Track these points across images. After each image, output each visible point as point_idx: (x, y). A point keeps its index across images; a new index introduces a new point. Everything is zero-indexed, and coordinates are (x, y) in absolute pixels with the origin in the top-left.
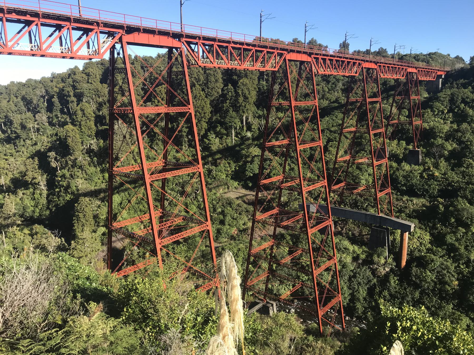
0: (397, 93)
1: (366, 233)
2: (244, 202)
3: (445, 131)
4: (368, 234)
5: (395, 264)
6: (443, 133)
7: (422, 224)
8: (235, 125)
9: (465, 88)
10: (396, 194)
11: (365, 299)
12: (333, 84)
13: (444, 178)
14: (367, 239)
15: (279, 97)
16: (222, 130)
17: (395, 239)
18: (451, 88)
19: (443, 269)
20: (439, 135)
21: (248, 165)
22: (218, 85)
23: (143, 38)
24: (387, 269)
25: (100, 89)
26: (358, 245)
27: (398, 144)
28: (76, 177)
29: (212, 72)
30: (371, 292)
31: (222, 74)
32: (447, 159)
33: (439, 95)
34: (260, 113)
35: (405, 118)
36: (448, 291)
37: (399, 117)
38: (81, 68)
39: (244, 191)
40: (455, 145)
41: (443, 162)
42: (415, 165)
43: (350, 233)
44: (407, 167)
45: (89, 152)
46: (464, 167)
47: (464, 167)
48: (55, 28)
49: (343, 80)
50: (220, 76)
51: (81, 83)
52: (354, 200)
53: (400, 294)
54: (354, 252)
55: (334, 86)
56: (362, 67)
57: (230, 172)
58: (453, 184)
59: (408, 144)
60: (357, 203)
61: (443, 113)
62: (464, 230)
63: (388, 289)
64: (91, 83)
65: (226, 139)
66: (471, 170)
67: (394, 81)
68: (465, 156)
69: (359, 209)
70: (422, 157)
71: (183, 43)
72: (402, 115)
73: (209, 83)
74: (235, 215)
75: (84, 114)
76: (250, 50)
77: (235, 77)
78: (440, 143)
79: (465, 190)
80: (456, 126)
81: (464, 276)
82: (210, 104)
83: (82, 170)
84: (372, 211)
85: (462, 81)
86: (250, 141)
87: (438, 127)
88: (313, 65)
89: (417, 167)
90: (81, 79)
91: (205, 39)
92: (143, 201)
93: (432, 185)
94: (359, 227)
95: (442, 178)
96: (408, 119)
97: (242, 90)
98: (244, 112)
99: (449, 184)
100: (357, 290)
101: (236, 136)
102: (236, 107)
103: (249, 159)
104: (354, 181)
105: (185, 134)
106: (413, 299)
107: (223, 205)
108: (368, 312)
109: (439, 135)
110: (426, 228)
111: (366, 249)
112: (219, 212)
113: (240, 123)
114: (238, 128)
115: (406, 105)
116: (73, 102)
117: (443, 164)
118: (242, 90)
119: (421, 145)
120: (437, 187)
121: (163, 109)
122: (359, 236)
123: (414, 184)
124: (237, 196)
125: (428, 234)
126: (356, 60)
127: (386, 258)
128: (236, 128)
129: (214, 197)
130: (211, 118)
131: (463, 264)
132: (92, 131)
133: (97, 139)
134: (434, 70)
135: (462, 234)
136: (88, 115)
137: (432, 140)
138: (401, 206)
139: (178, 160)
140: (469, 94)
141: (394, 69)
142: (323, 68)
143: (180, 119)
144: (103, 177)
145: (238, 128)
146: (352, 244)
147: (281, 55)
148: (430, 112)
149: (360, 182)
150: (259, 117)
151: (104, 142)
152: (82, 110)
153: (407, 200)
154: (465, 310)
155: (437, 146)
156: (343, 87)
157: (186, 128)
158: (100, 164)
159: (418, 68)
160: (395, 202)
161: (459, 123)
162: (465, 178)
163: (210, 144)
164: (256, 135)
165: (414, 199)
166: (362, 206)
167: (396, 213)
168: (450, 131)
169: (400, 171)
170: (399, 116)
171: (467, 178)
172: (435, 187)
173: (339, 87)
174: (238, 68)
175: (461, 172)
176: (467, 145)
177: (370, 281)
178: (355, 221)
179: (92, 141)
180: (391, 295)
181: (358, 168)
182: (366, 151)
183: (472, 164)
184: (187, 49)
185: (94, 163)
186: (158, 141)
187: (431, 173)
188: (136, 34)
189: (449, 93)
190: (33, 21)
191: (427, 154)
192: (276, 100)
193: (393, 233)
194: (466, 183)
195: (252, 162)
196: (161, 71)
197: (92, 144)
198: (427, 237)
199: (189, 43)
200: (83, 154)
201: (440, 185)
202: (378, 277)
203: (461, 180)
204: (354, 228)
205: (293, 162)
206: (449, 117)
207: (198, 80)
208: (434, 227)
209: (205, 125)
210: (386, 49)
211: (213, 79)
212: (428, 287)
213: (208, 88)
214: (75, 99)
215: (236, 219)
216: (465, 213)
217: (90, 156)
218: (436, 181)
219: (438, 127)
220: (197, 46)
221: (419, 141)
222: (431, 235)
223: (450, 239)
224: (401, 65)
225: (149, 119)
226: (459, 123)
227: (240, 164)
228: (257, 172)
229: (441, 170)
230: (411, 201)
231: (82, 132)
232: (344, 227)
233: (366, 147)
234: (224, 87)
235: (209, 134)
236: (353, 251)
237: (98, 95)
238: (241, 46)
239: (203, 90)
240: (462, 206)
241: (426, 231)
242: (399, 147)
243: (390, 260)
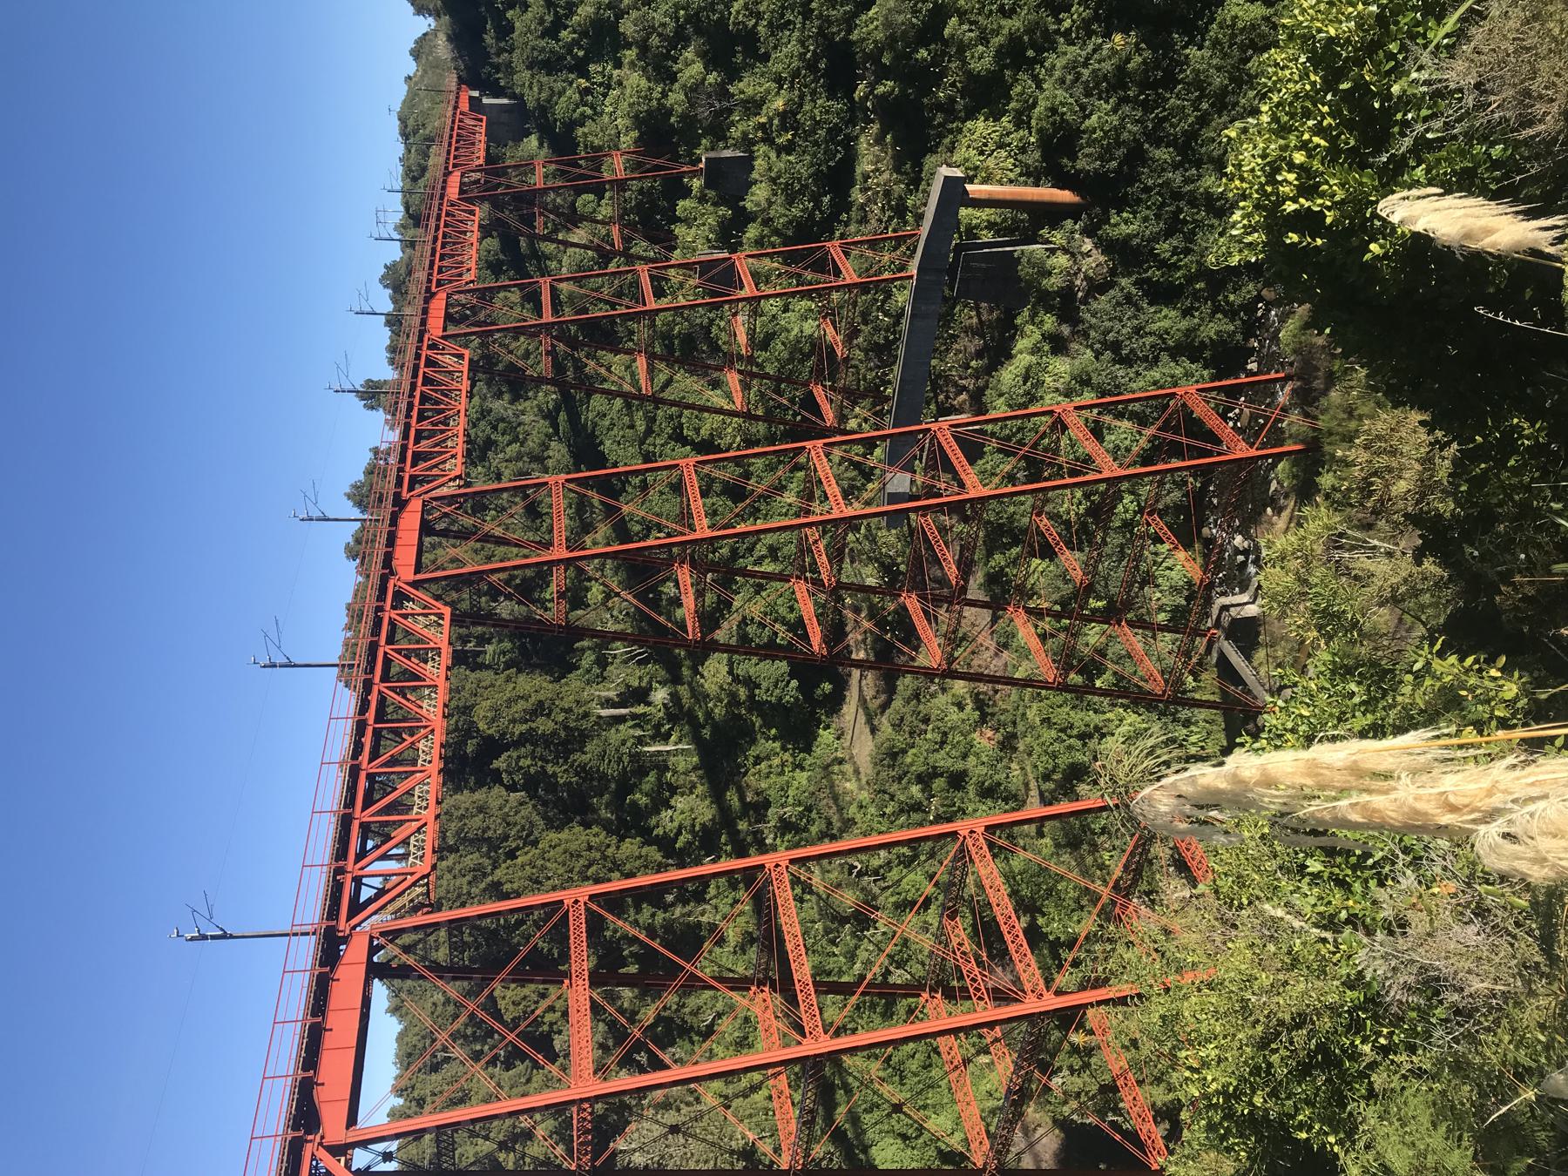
3: (644, 83)
5: (1069, 223)
11: (1187, 313)
13: (792, 83)
16: (646, 787)
17: (991, 226)
19: (1077, 80)
22: (494, 804)
24: (1088, 245)
29: (454, 826)
30: (1162, 294)
31: (458, 789)
32: (733, 75)
36: (1144, 62)
40: (689, 54)
46: (756, 24)
50: (465, 799)
53: (1163, 204)
56: (443, 337)
57: (787, 756)
59: (686, 192)
61: (587, 91)
63: (1149, 241)
65: (675, 772)
68: (723, 21)
70: (727, 147)
71: (354, 928)
73: (490, 834)
77: (471, 747)
80: (628, 53)
81: (1096, 18)
82: (559, 829)
85: (489, 39)
88: (434, 494)
91: (341, 852)
93: (813, 118)
94: (954, 338)
95: (792, 88)
96: (607, 195)
97: (513, 721)
99: (812, 66)
100: (1161, 337)
105: (660, 916)
106: (1175, 167)
107: (900, 779)
108: (1227, 302)
110: (951, 131)
111: (1026, 313)
112: (923, 791)
117: (747, 86)
118: (513, 721)
121: (578, 994)
122: (982, 336)
125: (969, 124)
127: (1053, 251)
129: (872, 810)
130: (607, 826)
131: (1060, 22)
135: (965, 27)
137: (673, 119)
139: (748, 940)
142: (444, 462)
143: (608, 934)
154: (1202, 9)
157: (638, 910)
163: (693, 826)
166: (887, 330)
169: (772, 213)
171: (789, 16)
172: (822, 108)
174: (439, 737)
177: (1129, 298)
180: (1168, 234)
182: (712, 321)
184: (375, 913)
186: (687, 1010)
188: (320, 1094)
196: (448, 1001)
198: (980, 127)
199: (356, 907)
201: (814, 93)
202: (1113, 272)
205: (751, 550)
207: (479, 872)
208: (948, 108)
209: (630, 847)
211: (477, 822)
212: (1137, 121)
213: (506, 838)
218: (801, 105)
220: (365, 880)
222: (971, 115)
223: (982, 60)
229: (768, 92)
230: (866, 177)
234: (502, 783)
235: (659, 831)
238: (369, 731)
239: (512, 855)
241: (960, 131)
243: (1058, 238)
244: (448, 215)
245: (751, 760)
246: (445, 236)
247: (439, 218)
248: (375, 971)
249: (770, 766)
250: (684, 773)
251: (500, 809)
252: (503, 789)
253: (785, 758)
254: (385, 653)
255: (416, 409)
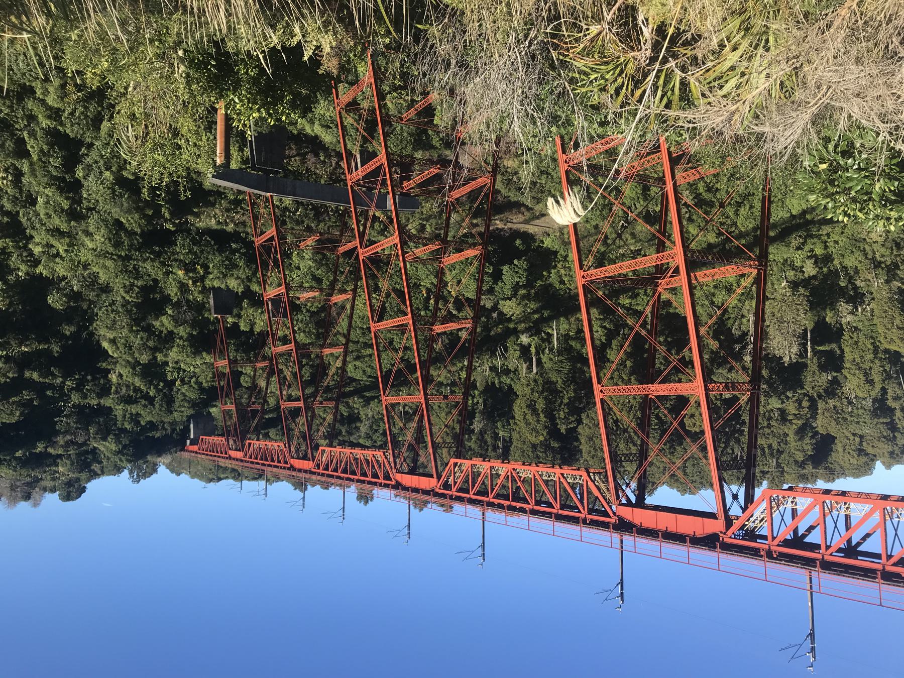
0: (259, 415)
1: (293, 159)
2: (529, 209)
3: (175, 349)
4: (290, 157)
6: (178, 346)
7: (197, 182)
8: (552, 357)
9: (151, 422)
10: (247, 233)
12: (376, 431)
13: (168, 266)
14: (290, 148)
15: (473, 407)
17: (241, 150)
18: (173, 424)
20: (184, 341)
21: (523, 281)
23: (688, 525)
25: (833, 423)
26: (306, 135)
27: (252, 325)
28: (889, 245)
31: (581, 451)
32: (167, 299)
33: (191, 412)
34: (506, 380)
35: (244, 371)
37: (255, 372)
38: (878, 464)
39: (531, 229)
40: (157, 324)
41: (172, 295)
42: (219, 288)
43: (322, 158)
44: (233, 284)
45: (856, 298)
47: (137, 286)
48: (860, 549)
49: (360, 437)
51: (876, 435)
52: (321, 221)
54: (312, 122)
55: (374, 427)
56: (313, 461)
58: (152, 257)
59: (236, 325)
60: (315, 215)
61: (182, 381)
62: (125, 173)
64: (854, 435)
65: (569, 330)
66: (125, 281)
67: (270, 434)
68: (137, 305)
69: (312, 204)
70: (208, 302)
71: (614, 513)
72: (250, 377)
74: (543, 182)
75: (866, 374)
76: (498, 496)
78: (181, 328)
79: (131, 246)
80: (159, 359)
83: (874, 259)
84: (288, 201)
85: (158, 435)
86: (522, 326)
87: (188, 356)
88: (393, 465)
89: (216, 284)
90: (876, 443)
92: (738, 199)
93: (187, 254)
94: (308, 170)
95: (171, 266)
96: (240, 369)
97: (538, 421)
98: (535, 381)
99: (158, 255)
101: (550, 336)
102: (549, 389)
103: (522, 292)
104: (324, 256)
109: (184, 341)
113: (543, 361)
114: (547, 351)
115: (245, 393)
116: (895, 399)
117: (173, 291)
118: (538, 421)
119: (213, 323)
120: (178, 250)
123: (217, 254)
124: (543, 219)
126: (323, 475)
128: (551, 350)
132: (850, 341)
133: (841, 325)
134: (204, 454)
136: (857, 372)
137: (195, 333)
138: (237, 213)
140: (142, 412)
141: (265, 456)
144: (826, 247)
145: (547, 351)
146: (316, 137)
147: (446, 486)
148: (204, 381)
149: (312, 254)
150: (507, 372)
151: (824, 318)
152: (871, 382)
153: (227, 224)
155: (186, 322)
156: (358, 424)
158: (835, 274)
159: (227, 458)
160: (247, 221)
161: (153, 362)
162: (134, 268)
163: (600, 319)
164: (512, 338)
165: (216, 227)
166: (306, 209)
167: (244, 199)
168: (167, 349)
169: (243, 276)
170: (255, 375)
171: (131, 268)
172: (181, 248)
173: (365, 425)
175: (142, 277)
176: (138, 325)
178: (316, 181)
179: (849, 319)
181: (319, 281)
182: (308, 311)
183: (126, 292)
185: (847, 274)
187: (191, 275)
188: (700, 533)
189: (175, 414)
190: (894, 565)
191: (200, 307)
192: (478, 403)
193: (245, 161)
194: (132, 259)
195: (516, 287)
197: (852, 313)
200: (871, 293)
201: (173, 253)
203: (140, 263)
204: (316, 168)
206: (172, 372)
210: (295, 489)
214: (891, 403)
215: (542, 172)
216: (125, 205)
217: (856, 288)
218: (181, 261)
219: (188, 356)
221: (216, 331)
224: (252, 463)
225: (728, 366)
226: (153, 362)
227: (539, 283)
228: (505, 269)
229: (174, 279)
230: (219, 223)
231: (872, 337)
232: (335, 169)
233: (308, 318)
234: (577, 427)
235: (603, 339)
236: (313, 123)
237: (837, 413)
240: (132, 218)
242: (250, 320)
244: (336, 470)
245: (562, 286)
246: (262, 459)
247: (258, 463)
248: (640, 503)
249: (565, 275)
250: (570, 325)
251: (590, 428)
252: (579, 427)
253: (560, 266)
254: (474, 494)
255: (350, 476)
